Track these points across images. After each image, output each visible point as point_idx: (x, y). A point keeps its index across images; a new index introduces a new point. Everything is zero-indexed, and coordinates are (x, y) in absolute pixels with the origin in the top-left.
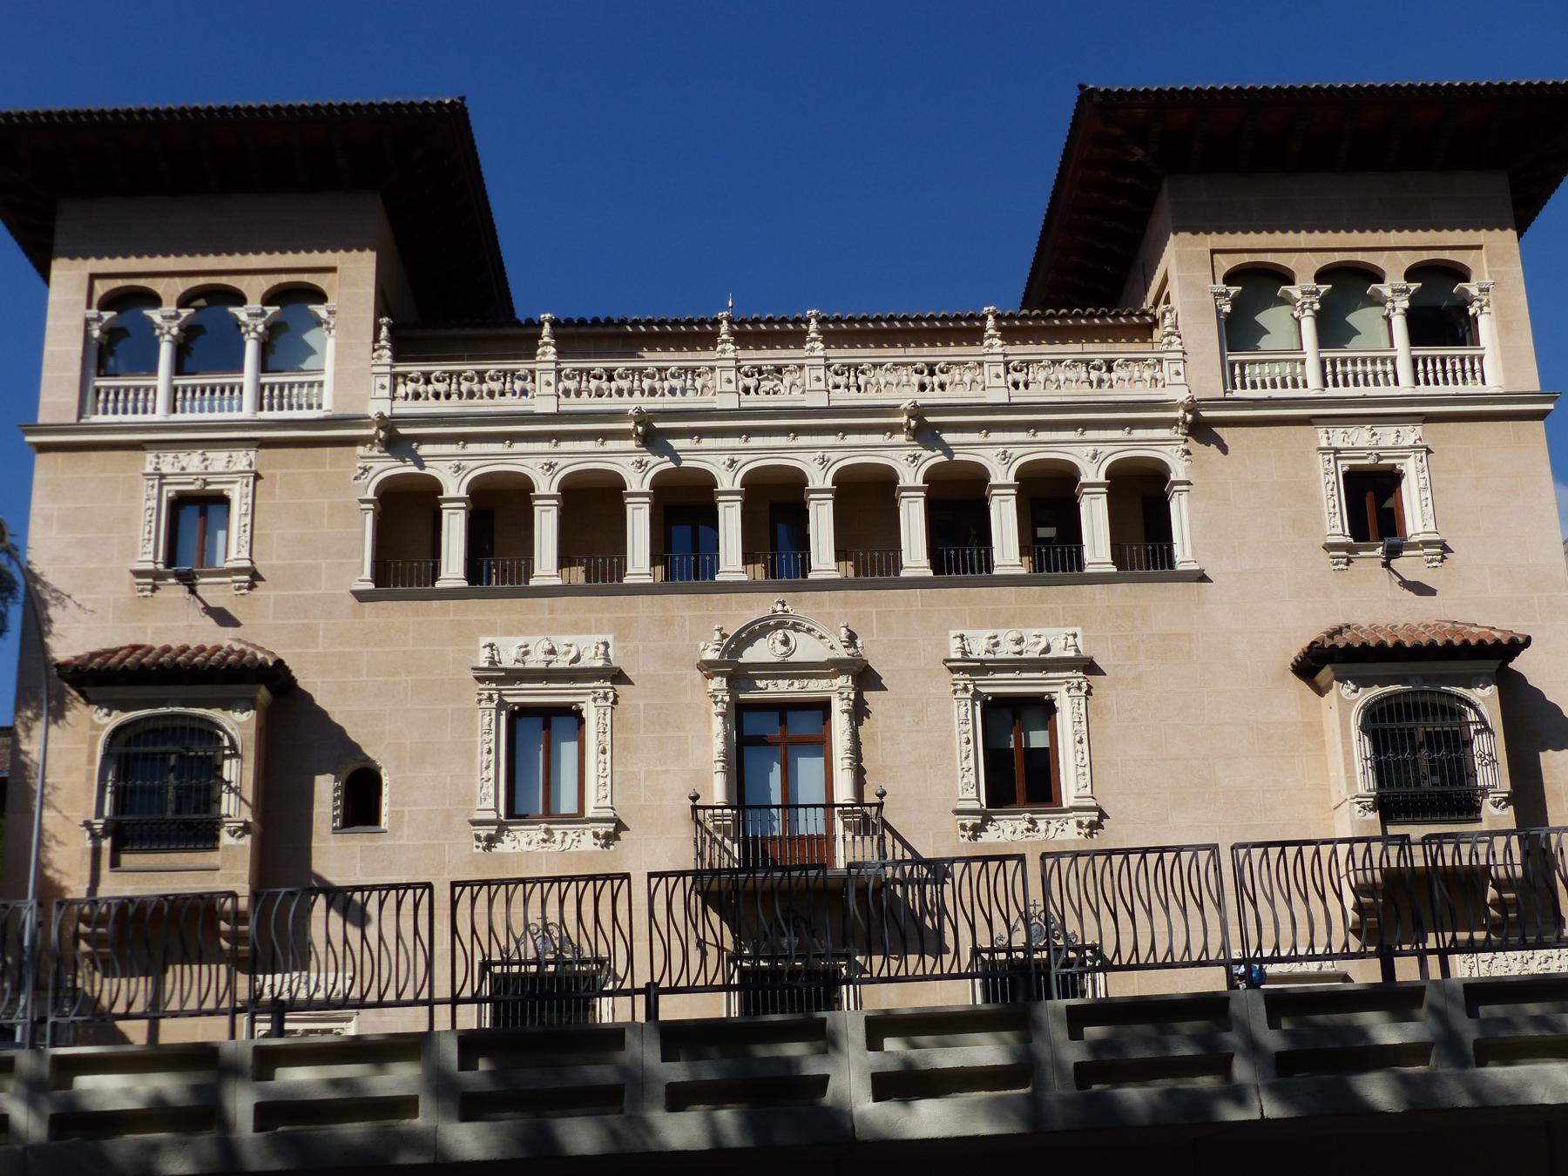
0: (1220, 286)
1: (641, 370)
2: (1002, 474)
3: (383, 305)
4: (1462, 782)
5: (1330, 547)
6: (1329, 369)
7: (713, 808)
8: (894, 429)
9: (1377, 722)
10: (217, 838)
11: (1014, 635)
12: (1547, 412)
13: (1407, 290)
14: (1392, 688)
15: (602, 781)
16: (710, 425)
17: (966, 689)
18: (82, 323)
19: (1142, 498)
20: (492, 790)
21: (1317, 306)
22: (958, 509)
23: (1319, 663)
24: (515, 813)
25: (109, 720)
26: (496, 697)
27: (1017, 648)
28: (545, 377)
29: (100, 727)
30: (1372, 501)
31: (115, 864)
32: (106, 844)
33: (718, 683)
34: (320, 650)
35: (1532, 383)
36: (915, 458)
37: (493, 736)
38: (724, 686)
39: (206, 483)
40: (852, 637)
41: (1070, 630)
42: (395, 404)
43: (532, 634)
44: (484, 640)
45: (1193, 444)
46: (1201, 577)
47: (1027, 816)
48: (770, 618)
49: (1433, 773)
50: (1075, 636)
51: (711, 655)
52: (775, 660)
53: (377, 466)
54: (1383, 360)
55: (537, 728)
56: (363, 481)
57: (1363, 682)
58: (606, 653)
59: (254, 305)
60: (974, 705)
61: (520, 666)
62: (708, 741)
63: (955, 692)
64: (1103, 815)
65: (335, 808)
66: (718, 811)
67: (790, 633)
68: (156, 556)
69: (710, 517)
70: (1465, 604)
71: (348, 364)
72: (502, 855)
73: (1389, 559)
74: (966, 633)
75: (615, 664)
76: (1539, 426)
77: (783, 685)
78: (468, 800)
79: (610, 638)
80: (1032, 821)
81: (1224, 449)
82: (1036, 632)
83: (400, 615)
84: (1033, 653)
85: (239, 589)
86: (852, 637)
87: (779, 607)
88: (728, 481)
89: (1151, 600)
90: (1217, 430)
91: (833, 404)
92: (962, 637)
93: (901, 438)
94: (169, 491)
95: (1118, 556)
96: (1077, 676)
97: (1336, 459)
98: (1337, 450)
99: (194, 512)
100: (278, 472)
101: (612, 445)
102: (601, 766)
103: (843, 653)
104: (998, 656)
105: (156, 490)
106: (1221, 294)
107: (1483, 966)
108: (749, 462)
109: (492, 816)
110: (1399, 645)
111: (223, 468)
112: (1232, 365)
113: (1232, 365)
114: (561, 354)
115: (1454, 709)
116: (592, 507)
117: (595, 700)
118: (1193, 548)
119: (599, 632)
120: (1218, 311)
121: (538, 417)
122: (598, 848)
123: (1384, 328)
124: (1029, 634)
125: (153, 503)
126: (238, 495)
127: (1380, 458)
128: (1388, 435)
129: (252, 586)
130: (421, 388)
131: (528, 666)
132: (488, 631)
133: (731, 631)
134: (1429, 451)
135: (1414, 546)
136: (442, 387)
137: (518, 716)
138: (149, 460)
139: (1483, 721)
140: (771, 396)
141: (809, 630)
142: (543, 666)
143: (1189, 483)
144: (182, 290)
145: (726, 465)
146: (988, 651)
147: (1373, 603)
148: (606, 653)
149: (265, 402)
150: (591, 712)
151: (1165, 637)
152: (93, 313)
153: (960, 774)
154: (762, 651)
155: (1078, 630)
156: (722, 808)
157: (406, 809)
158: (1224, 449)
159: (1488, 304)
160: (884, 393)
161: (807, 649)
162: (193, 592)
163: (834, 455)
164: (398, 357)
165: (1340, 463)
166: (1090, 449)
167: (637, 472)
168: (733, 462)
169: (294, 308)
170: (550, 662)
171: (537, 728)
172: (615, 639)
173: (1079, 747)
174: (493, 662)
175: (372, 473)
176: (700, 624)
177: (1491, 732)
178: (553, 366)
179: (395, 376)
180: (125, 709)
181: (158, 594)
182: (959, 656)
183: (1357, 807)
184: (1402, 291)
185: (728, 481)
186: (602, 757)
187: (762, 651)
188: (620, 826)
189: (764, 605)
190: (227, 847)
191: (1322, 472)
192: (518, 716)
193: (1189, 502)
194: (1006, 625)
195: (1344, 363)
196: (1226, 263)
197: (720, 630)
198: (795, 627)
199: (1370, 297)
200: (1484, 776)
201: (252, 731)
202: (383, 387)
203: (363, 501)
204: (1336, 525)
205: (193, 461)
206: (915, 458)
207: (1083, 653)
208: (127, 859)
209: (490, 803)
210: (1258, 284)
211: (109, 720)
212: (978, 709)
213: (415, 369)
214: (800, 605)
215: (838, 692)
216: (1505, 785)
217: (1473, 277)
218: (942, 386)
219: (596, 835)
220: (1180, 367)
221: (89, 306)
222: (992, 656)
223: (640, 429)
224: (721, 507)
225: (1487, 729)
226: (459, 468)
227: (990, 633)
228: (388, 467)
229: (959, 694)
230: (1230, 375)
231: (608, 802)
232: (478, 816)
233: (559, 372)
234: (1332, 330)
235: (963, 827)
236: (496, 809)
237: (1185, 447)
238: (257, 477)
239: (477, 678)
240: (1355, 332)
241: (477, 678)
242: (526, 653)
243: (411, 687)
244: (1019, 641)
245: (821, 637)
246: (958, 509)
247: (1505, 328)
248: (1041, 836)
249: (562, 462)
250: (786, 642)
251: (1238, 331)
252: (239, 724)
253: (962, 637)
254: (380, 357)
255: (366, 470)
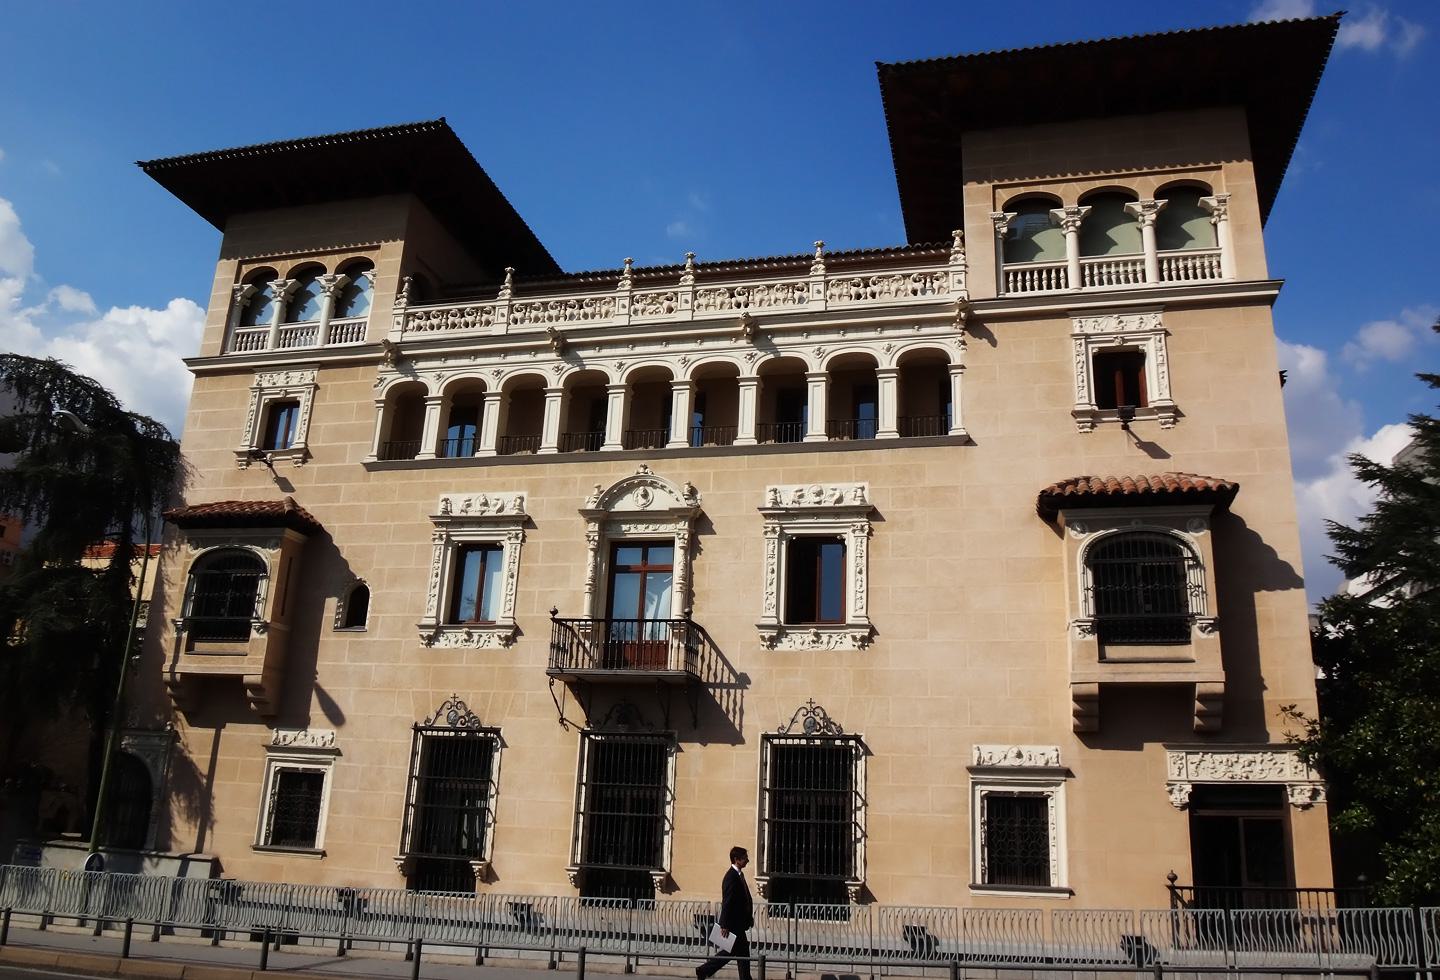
0: (999, 213)
1: (793, 285)
2: (816, 366)
3: (405, 269)
4: (1179, 611)
5: (1076, 414)
6: (1087, 272)
7: (580, 620)
8: (736, 336)
9: (1096, 558)
10: (1188, 635)
11: (816, 489)
12: (1274, 297)
13: (1155, 206)
14: (1102, 532)
15: (859, 595)
16: (608, 337)
17: (774, 531)
18: (230, 292)
19: (927, 385)
20: (435, 603)
21: (1078, 223)
22: (783, 392)
23: (1058, 506)
24: (453, 618)
25: (1088, 538)
26: (778, 529)
27: (817, 499)
28: (816, 287)
29: (190, 556)
30: (1118, 380)
31: (190, 649)
32: (185, 635)
33: (594, 527)
34: (340, 504)
35: (1261, 274)
36: (752, 356)
37: (775, 560)
38: (597, 529)
39: (287, 393)
40: (693, 492)
41: (860, 485)
42: (405, 334)
43: (473, 491)
44: (769, 488)
45: (968, 337)
46: (968, 441)
47: (813, 630)
48: (634, 478)
49: (1147, 601)
50: (863, 489)
51: (591, 506)
52: (637, 509)
53: (390, 377)
54: (1134, 263)
55: (469, 556)
56: (380, 388)
57: (1087, 526)
58: (521, 504)
59: (1071, 204)
60: (780, 544)
61: (464, 514)
62: (583, 570)
63: (766, 533)
64: (873, 631)
65: (337, 614)
66: (583, 623)
67: (650, 490)
68: (1090, 400)
69: (871, 394)
70: (1194, 457)
71: (382, 311)
72: (438, 650)
73: (1125, 422)
74: (779, 488)
75: (526, 513)
76: (1265, 310)
77: (641, 528)
78: (420, 610)
79: (525, 494)
80: (817, 635)
81: (994, 343)
82: (833, 486)
83: (394, 480)
84: (829, 502)
85: (296, 463)
86: (693, 492)
87: (642, 470)
88: (617, 378)
89: (929, 461)
90: (988, 325)
91: (695, 319)
92: (775, 491)
93: (743, 343)
94: (266, 399)
95: (761, 433)
96: (862, 521)
97: (1087, 343)
98: (1087, 336)
99: (279, 410)
100: (329, 384)
101: (541, 356)
102: (859, 583)
103: (683, 504)
104: (802, 505)
105: (1083, 347)
106: (999, 219)
107: (1222, 768)
108: (633, 364)
109: (774, 622)
110: (1178, 490)
111: (296, 381)
112: (1007, 274)
113: (1007, 274)
114: (517, 292)
115: (1172, 550)
116: (715, 390)
117: (854, 531)
118: (963, 417)
119: (518, 490)
120: (996, 232)
121: (501, 338)
122: (502, 647)
123: (1137, 241)
124: (827, 488)
125: (254, 407)
126: (304, 399)
127: (1124, 341)
128: (1132, 322)
129: (304, 461)
130: (861, 290)
131: (469, 514)
132: (446, 490)
133: (606, 488)
134: (1167, 334)
135: (1151, 412)
136: (435, 322)
137: (462, 551)
138: (1075, 325)
139: (1195, 558)
140: (653, 316)
141: (663, 487)
142: (478, 514)
143: (963, 367)
144: (1157, 186)
145: (615, 367)
146: (462, 511)
147: (1111, 458)
148: (521, 504)
149: (1011, 285)
150: (507, 545)
151: (934, 489)
152: (237, 286)
153: (765, 596)
154: (629, 503)
155: (866, 485)
156: (586, 621)
157: (381, 615)
158: (994, 343)
159: (1225, 213)
160: (774, 307)
161: (661, 501)
162: (1126, 427)
163: (693, 357)
164: (412, 302)
165: (1090, 346)
166: (885, 344)
167: (747, 362)
168: (621, 365)
169: (1034, 219)
170: (484, 512)
171: (469, 556)
172: (529, 495)
173: (859, 576)
174: (776, 502)
175: (386, 382)
176: (585, 482)
177: (1203, 568)
178: (690, 288)
179: (407, 316)
180: (1092, 531)
181: (250, 467)
182: (770, 505)
183: (1078, 630)
184: (1150, 207)
185: (617, 378)
186: (510, 580)
187: (629, 503)
188: (517, 632)
189: (630, 469)
190: (1200, 641)
191: (1075, 353)
192: (462, 551)
193: (962, 382)
194: (810, 481)
195: (1100, 266)
196: (1005, 195)
197: (599, 487)
198: (653, 484)
199: (1200, 208)
200: (1195, 605)
201: (278, 560)
202: (398, 323)
203: (378, 402)
204: (1083, 395)
205: (280, 379)
206: (752, 356)
207: (869, 502)
208: (199, 646)
209: (433, 613)
210: (1035, 208)
211: (1088, 538)
212: (784, 547)
213: (420, 310)
214: (660, 469)
215: (678, 530)
216: (1213, 612)
217: (1215, 194)
218: (873, 295)
219: (854, 638)
220: (962, 277)
221: (236, 281)
222: (797, 506)
223: (963, 315)
224: (810, 385)
225: (1198, 565)
226: (439, 376)
227: (798, 487)
228: (395, 378)
229: (437, 542)
230: (1004, 280)
231: (863, 612)
232: (425, 622)
233: (827, 283)
234: (1092, 240)
235: (763, 638)
236: (778, 617)
237: (961, 339)
238: (317, 387)
239: (765, 516)
240: (1039, 249)
241: (765, 516)
242: (469, 506)
243: (387, 529)
244: (819, 493)
245: (671, 492)
246: (783, 392)
247: (1239, 230)
248: (824, 647)
249: (507, 369)
250: (645, 495)
251: (1013, 246)
252: (270, 556)
253: (775, 491)
254: (400, 303)
255: (381, 380)
